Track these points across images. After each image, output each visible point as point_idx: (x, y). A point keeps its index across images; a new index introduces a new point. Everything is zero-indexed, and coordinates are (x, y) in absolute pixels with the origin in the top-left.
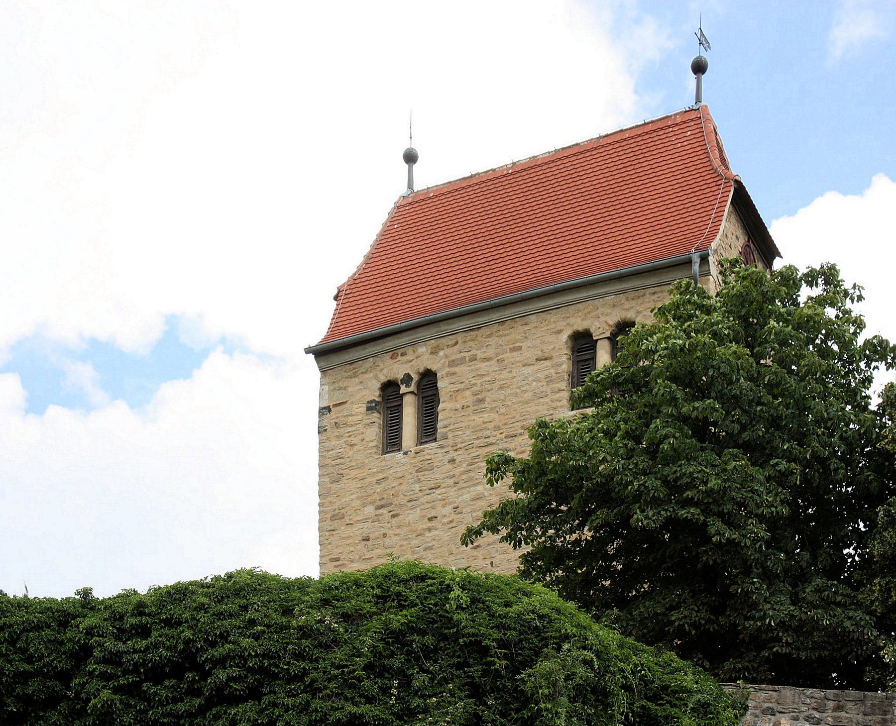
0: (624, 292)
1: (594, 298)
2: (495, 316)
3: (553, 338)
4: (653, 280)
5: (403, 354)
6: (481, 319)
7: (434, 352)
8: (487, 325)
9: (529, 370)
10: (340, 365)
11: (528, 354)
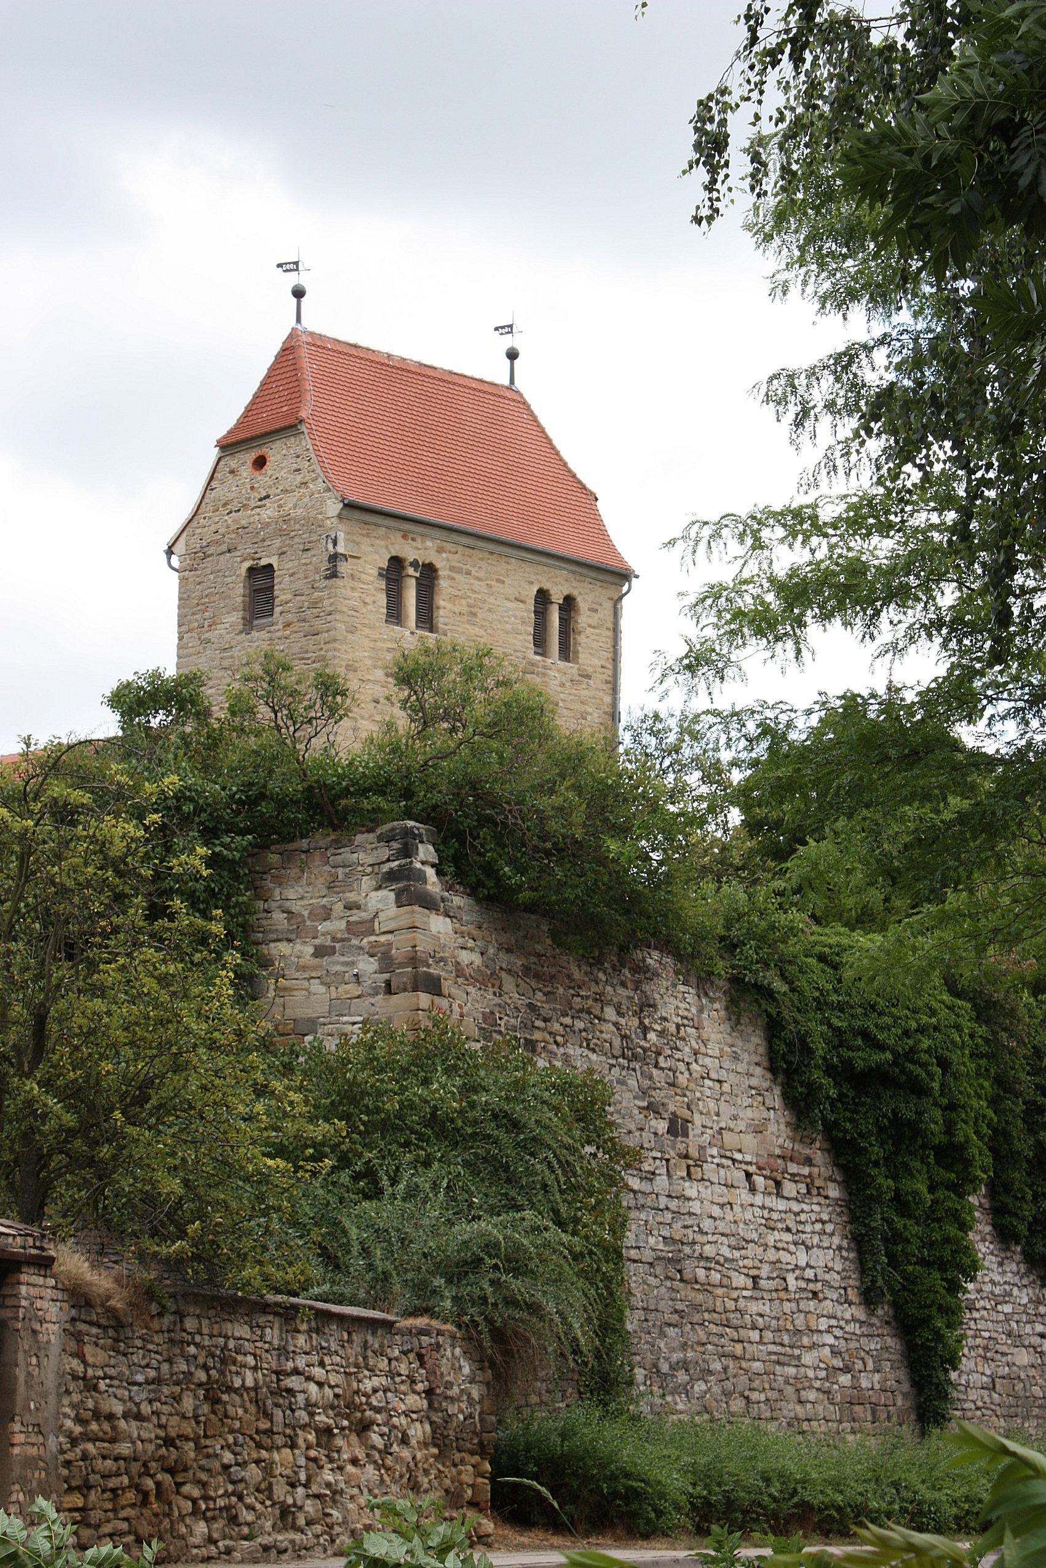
0: (574, 572)
1: (555, 567)
2: (491, 547)
3: (527, 586)
4: (593, 574)
5: (413, 539)
6: (480, 544)
7: (440, 550)
8: (481, 549)
9: (509, 604)
10: (357, 520)
11: (510, 591)
